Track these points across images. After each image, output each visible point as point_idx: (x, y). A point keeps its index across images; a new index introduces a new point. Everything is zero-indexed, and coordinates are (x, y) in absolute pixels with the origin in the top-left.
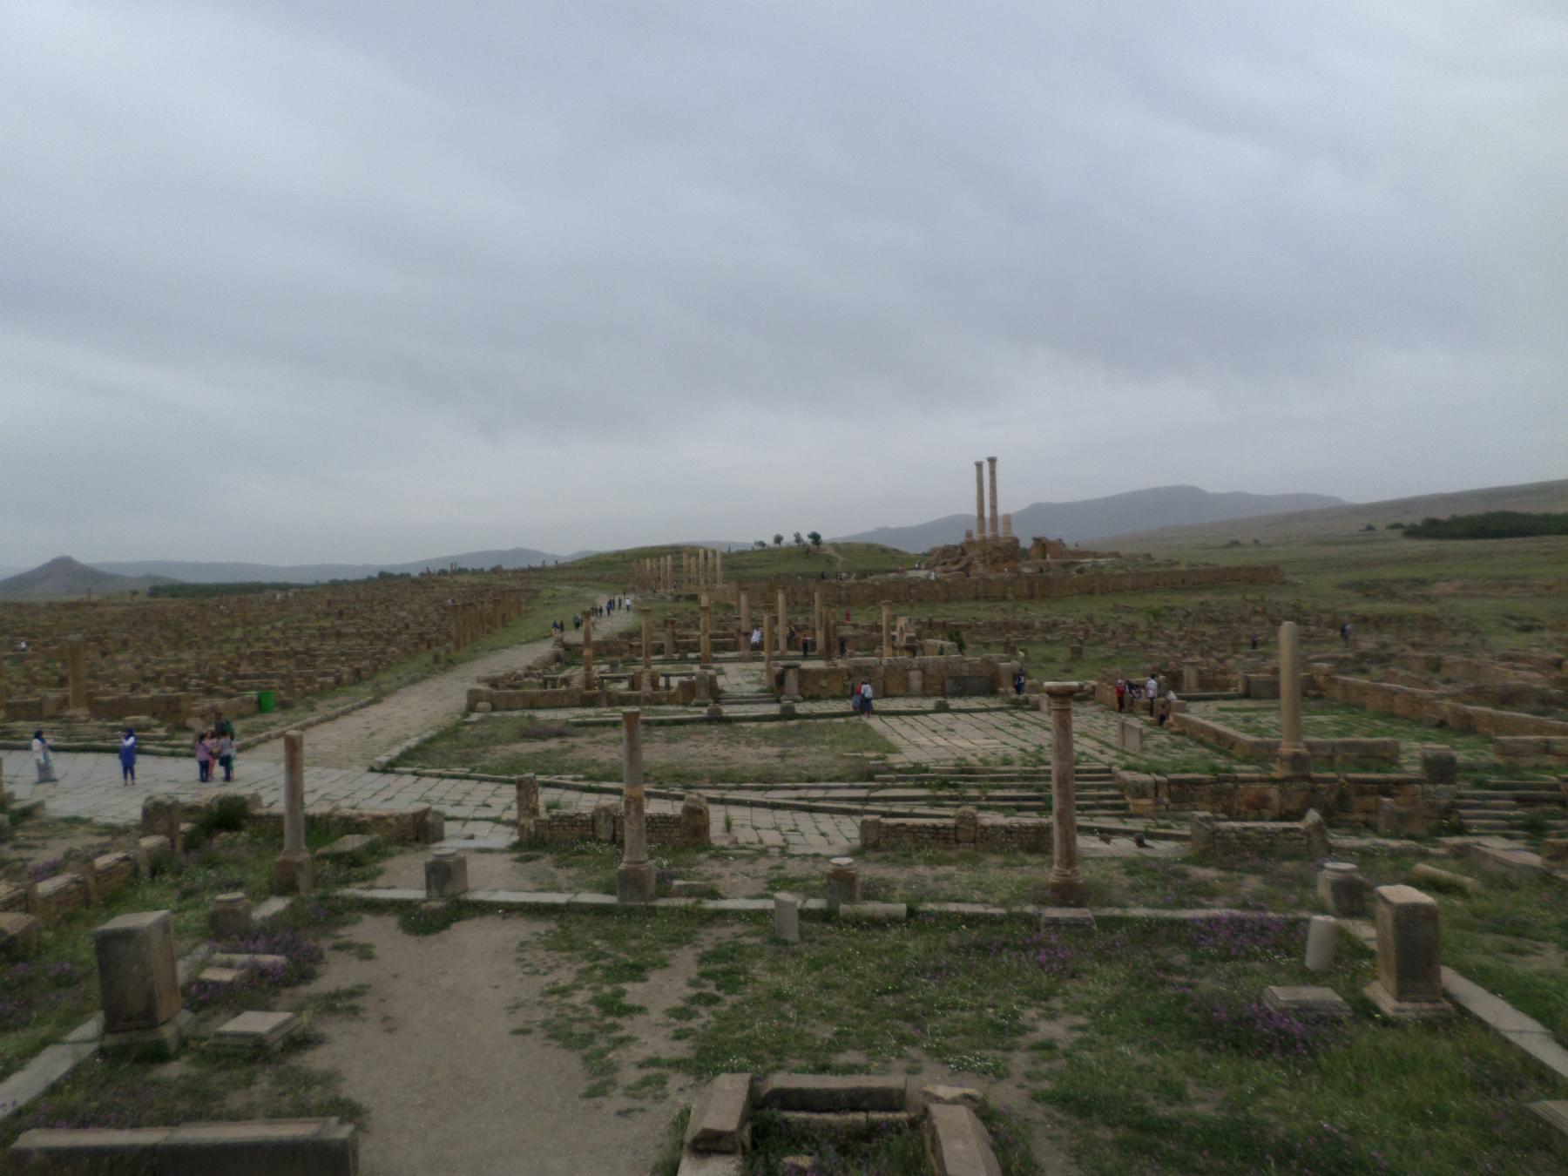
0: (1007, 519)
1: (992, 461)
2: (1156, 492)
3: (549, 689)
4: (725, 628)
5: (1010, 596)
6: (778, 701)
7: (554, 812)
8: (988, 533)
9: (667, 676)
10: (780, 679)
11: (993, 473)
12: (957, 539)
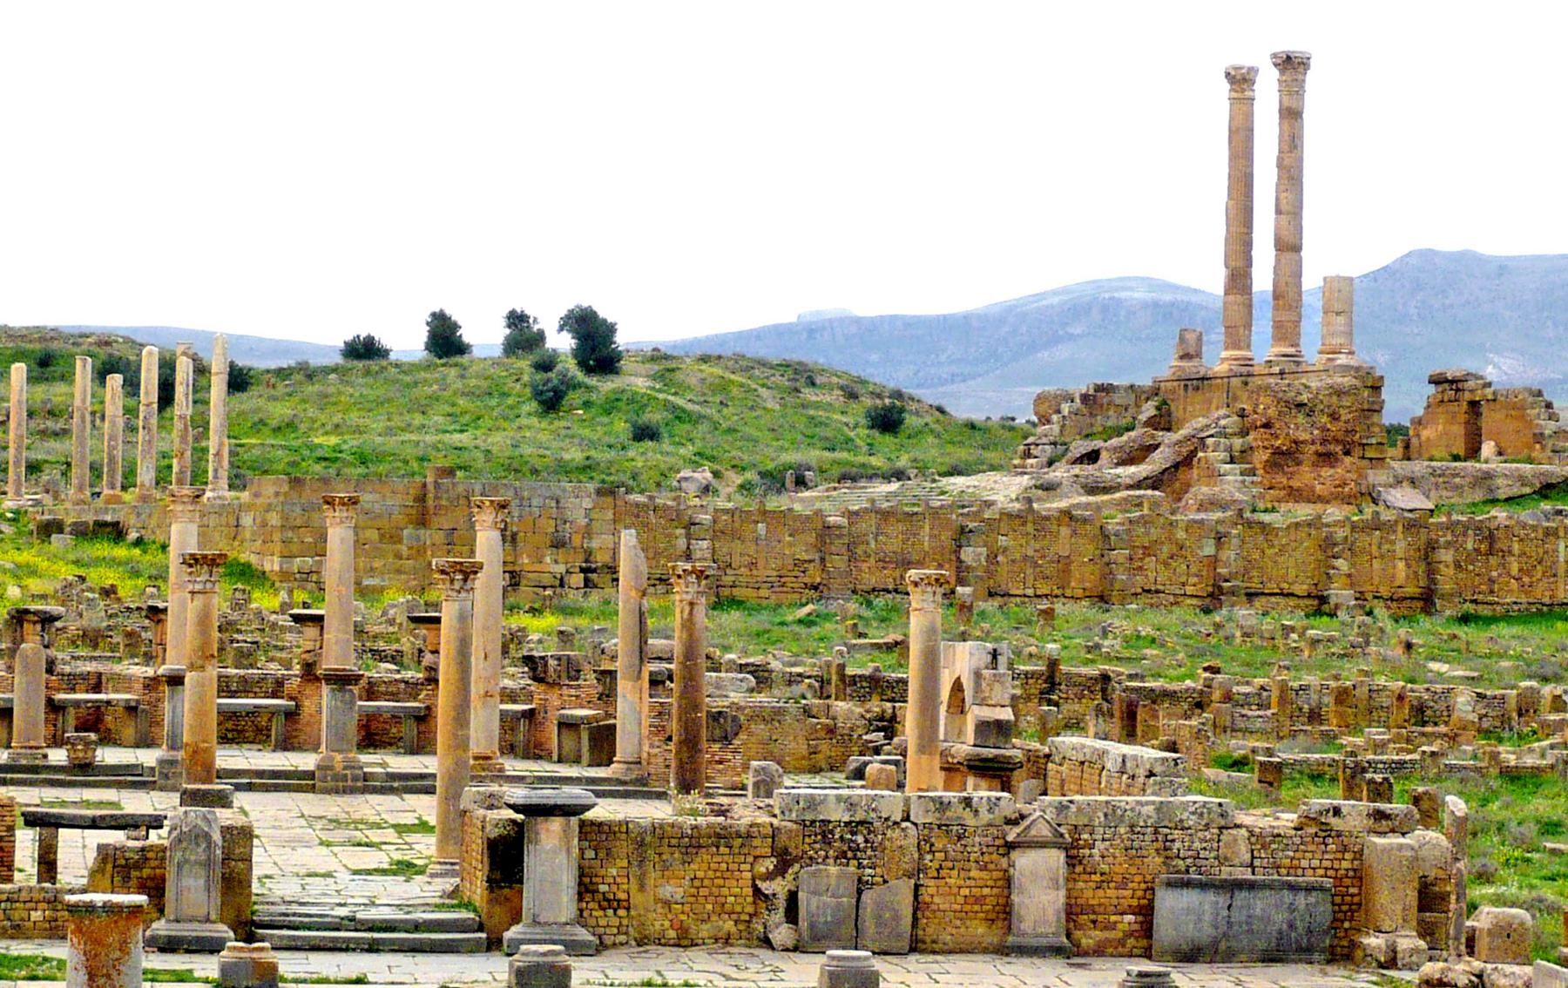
0: (1340, 295)
1: (1292, 65)
2: (162, 328)
3: (618, 666)
4: (245, 657)
5: (1340, 593)
6: (493, 944)
7: (1061, 881)
8: (1264, 348)
9: (45, 822)
10: (506, 859)
11: (1291, 115)
12: (1150, 365)
